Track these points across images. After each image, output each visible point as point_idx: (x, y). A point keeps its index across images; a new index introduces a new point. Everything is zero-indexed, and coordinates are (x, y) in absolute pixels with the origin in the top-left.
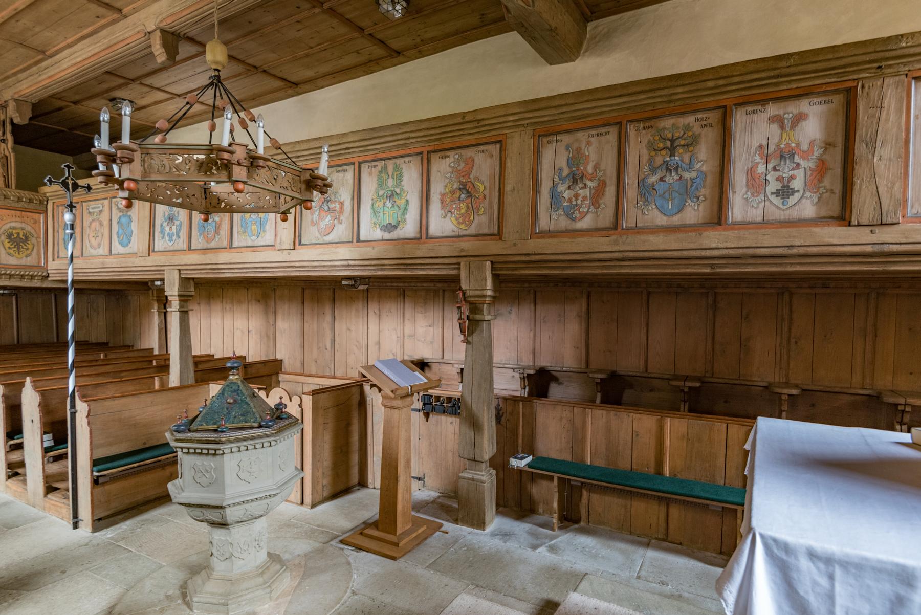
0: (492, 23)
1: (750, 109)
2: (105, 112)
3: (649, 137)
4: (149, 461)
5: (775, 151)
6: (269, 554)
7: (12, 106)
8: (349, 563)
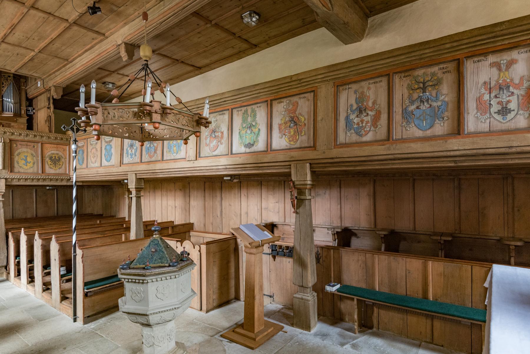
0: (308, 22)
1: (476, 59)
2: (83, 87)
3: (408, 82)
4: (107, 285)
5: (495, 85)
6: (177, 343)
7: (53, 89)
8: (225, 351)
